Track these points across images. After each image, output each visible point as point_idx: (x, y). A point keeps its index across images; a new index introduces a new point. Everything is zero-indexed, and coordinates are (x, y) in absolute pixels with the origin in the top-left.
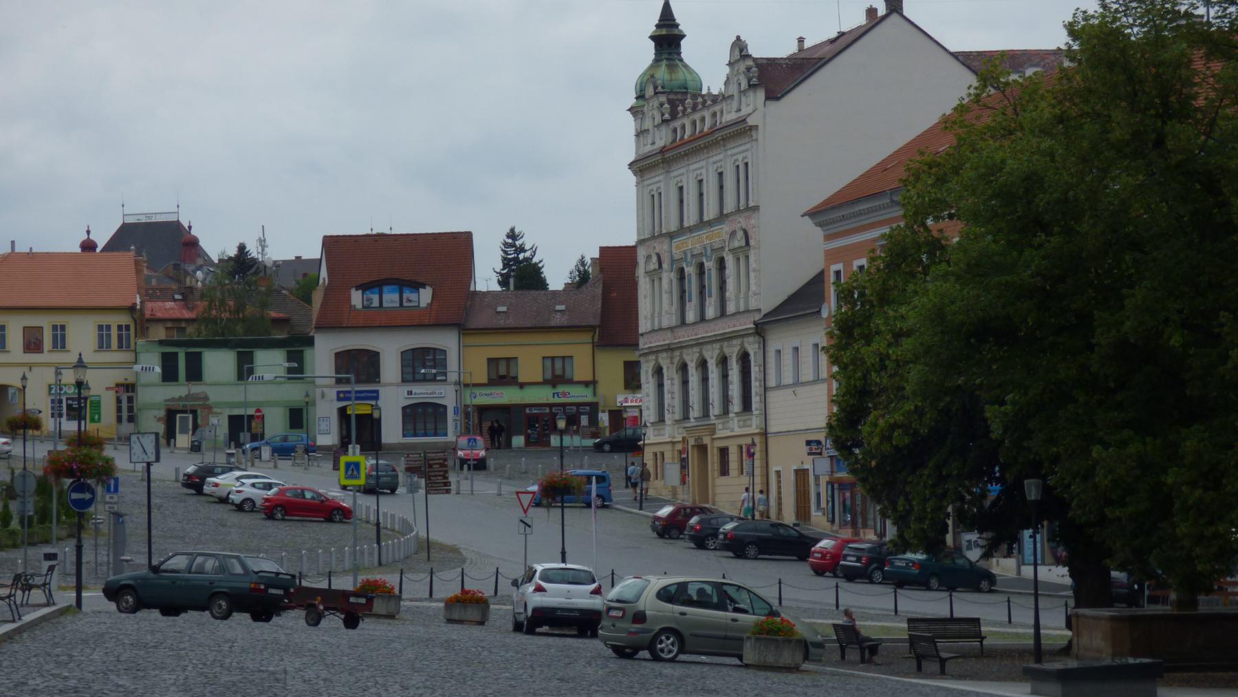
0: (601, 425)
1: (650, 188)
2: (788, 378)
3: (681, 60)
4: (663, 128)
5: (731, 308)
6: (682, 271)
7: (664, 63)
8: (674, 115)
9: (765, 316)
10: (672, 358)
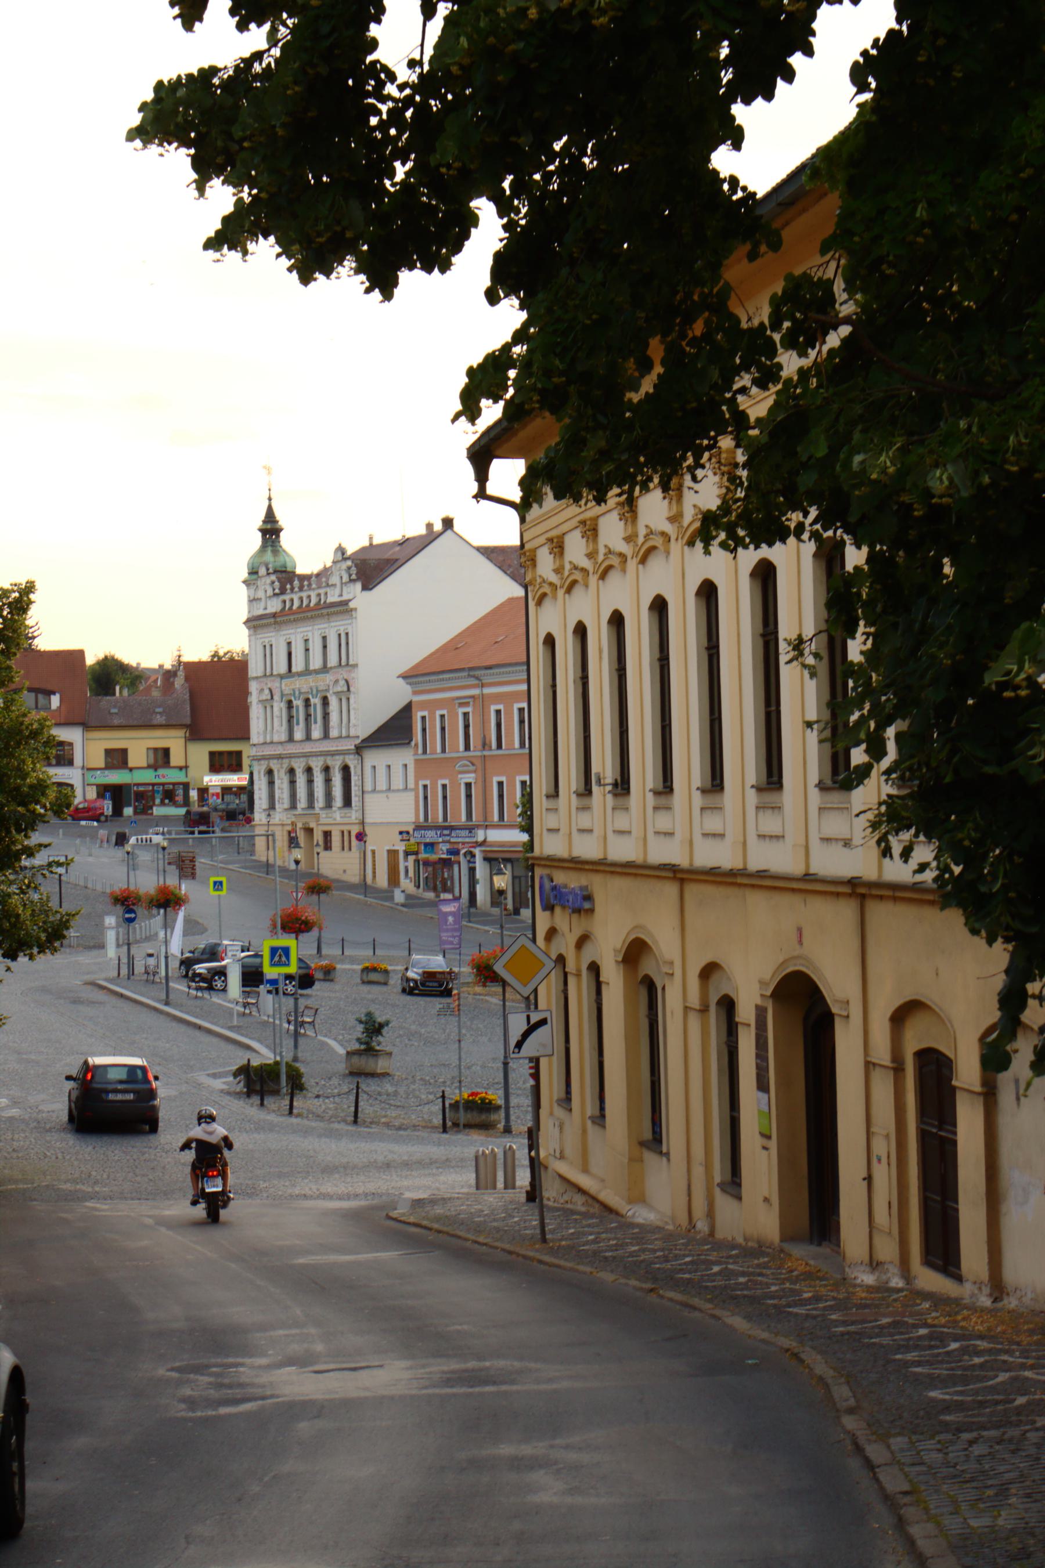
0: (191, 800)
1: (263, 640)
2: (382, 785)
3: (281, 547)
4: (275, 599)
5: (334, 733)
6: (290, 702)
7: (270, 549)
9: (363, 741)
10: (282, 764)
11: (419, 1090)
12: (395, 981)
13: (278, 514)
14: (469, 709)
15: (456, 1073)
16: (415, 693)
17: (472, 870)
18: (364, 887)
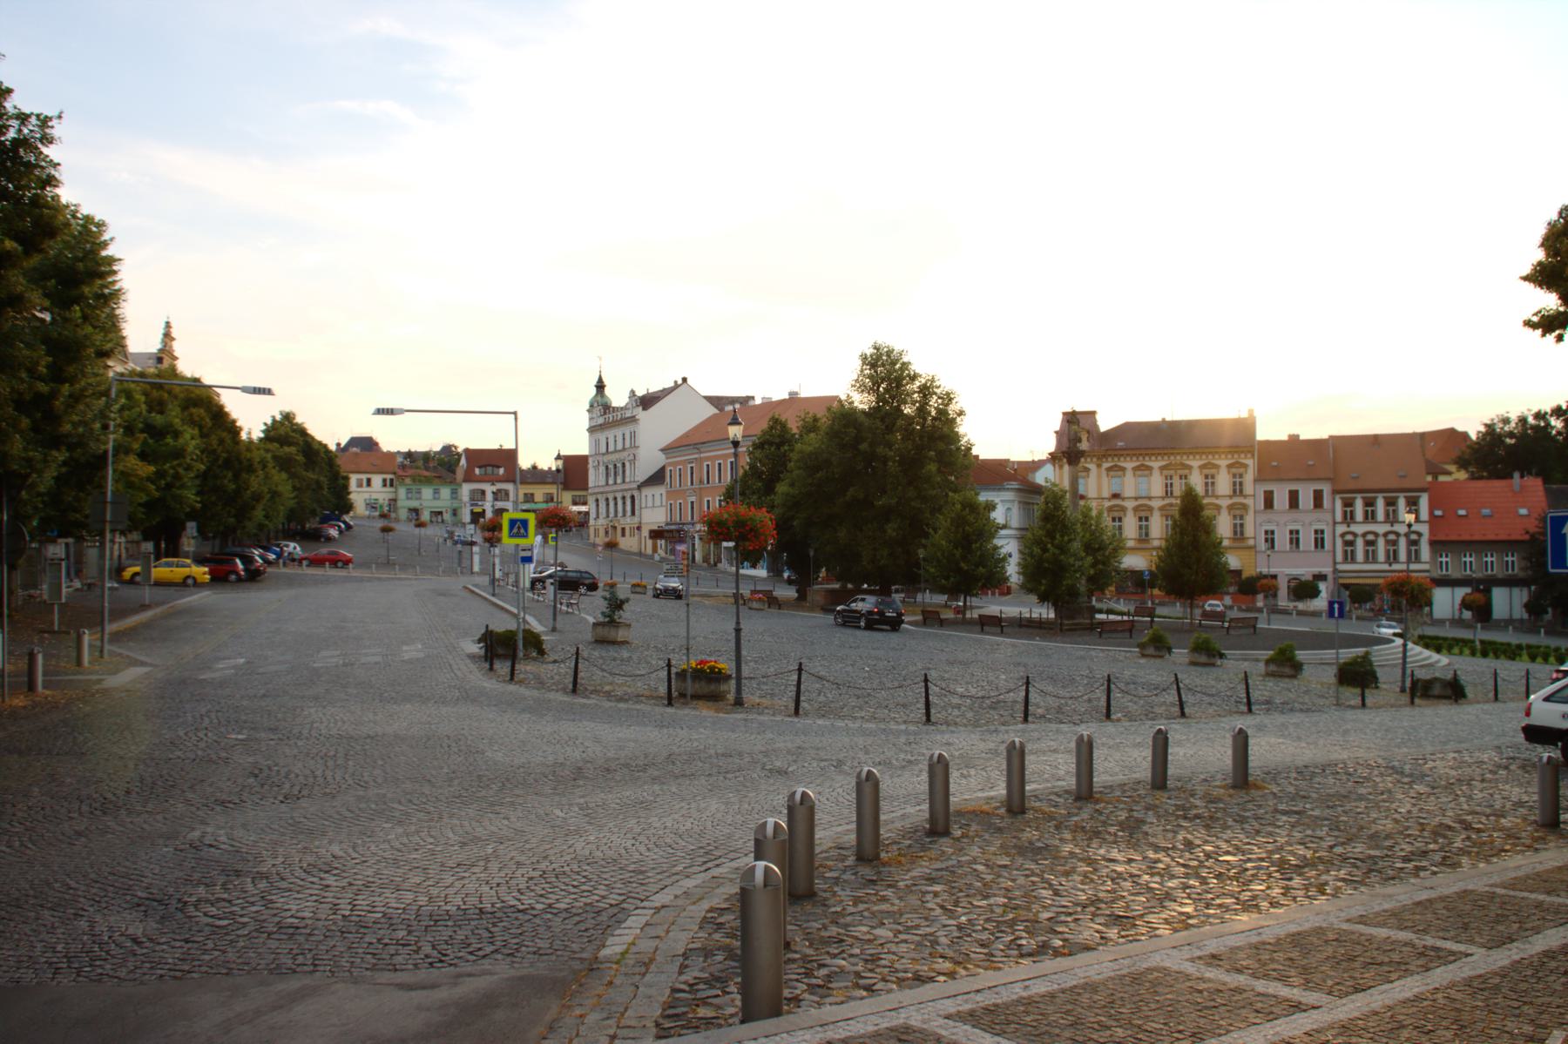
2: (650, 504)
5: (627, 480)
8: (605, 413)
11: (651, 656)
12: (650, 593)
13: (604, 380)
14: (693, 465)
15: (684, 642)
16: (667, 458)
17: (694, 545)
18: (640, 554)
